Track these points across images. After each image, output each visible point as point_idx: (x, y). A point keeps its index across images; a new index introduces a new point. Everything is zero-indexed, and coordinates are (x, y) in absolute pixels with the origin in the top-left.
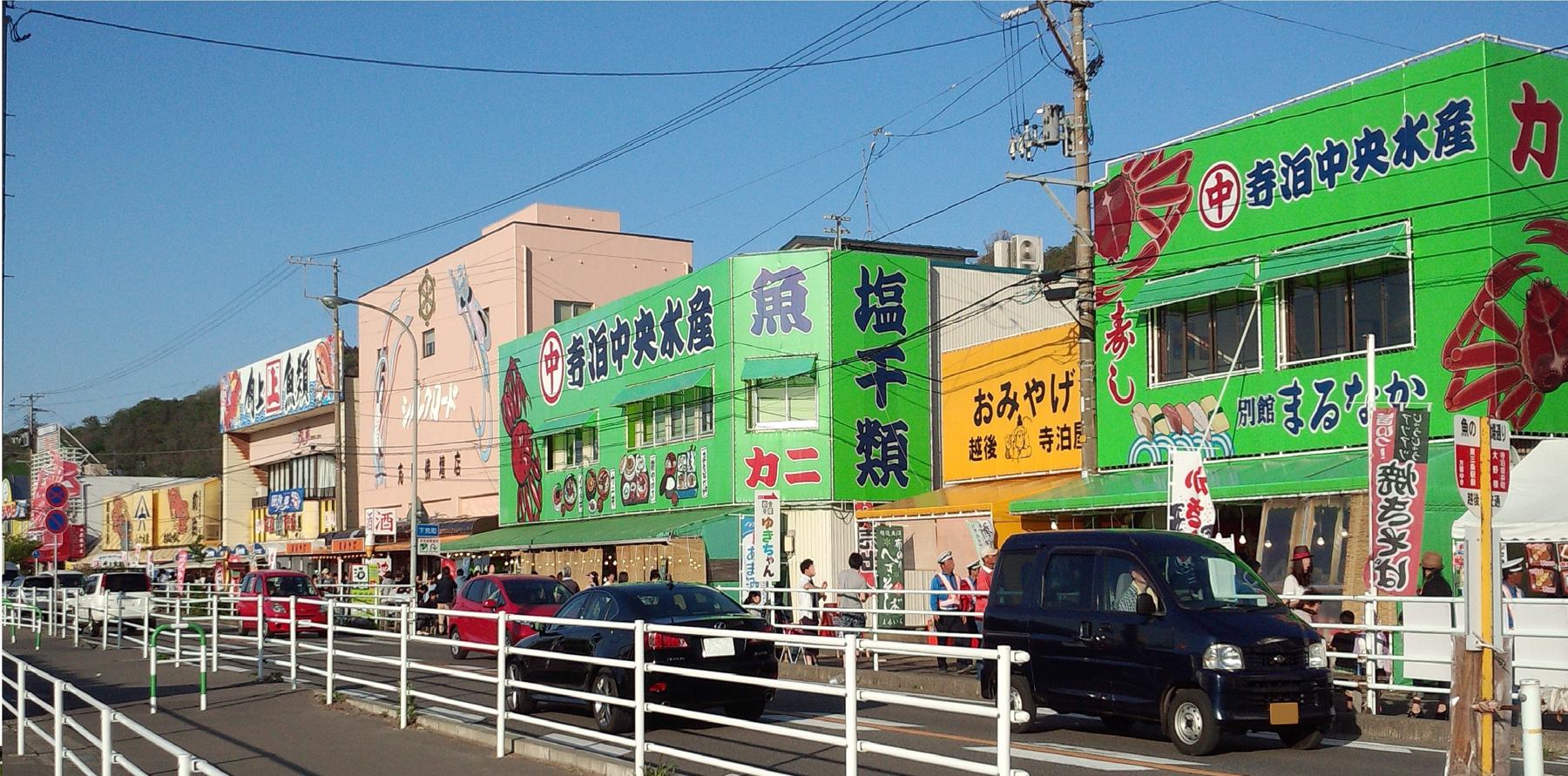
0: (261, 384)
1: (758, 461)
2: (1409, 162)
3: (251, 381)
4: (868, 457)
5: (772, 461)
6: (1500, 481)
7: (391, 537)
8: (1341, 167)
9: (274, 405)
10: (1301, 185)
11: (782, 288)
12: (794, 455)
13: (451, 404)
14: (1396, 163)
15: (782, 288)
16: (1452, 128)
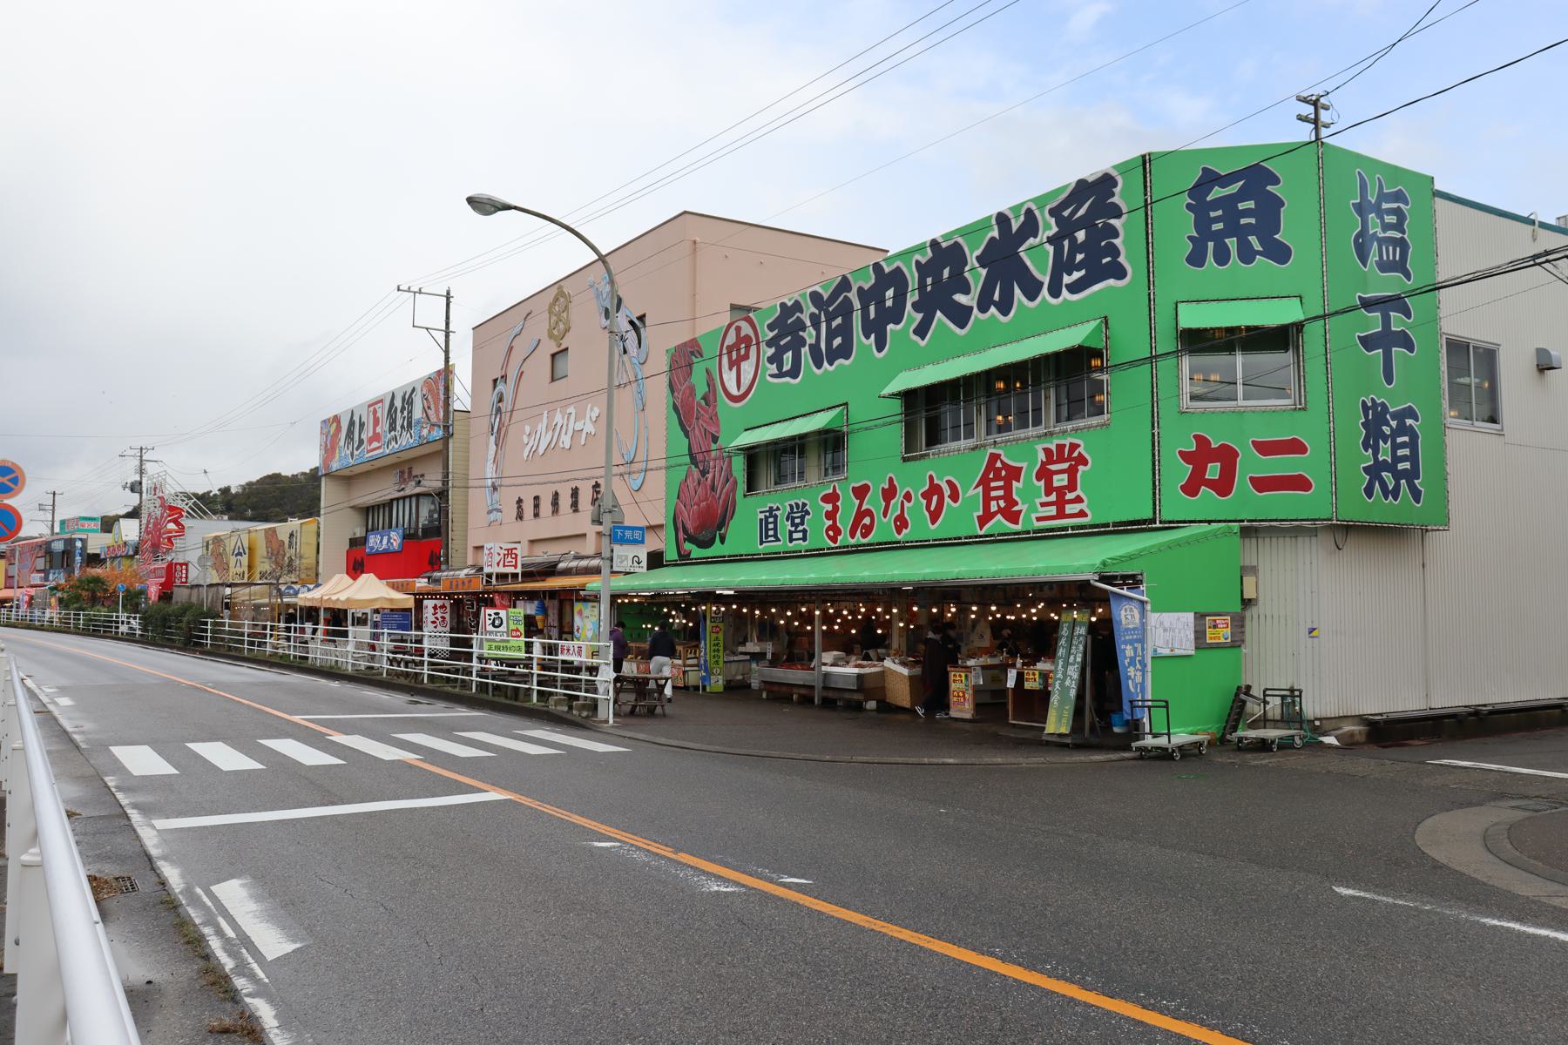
0: (362, 425)
1: (1201, 454)
2: (1005, 307)
3: (352, 423)
4: (1375, 454)
5: (1227, 456)
6: (224, 1000)
7: (515, 576)
8: (896, 315)
9: (375, 444)
10: (837, 341)
11: (1242, 195)
12: (1265, 448)
13: (589, 428)
14: (983, 308)
15: (1242, 195)
16: (1081, 235)
